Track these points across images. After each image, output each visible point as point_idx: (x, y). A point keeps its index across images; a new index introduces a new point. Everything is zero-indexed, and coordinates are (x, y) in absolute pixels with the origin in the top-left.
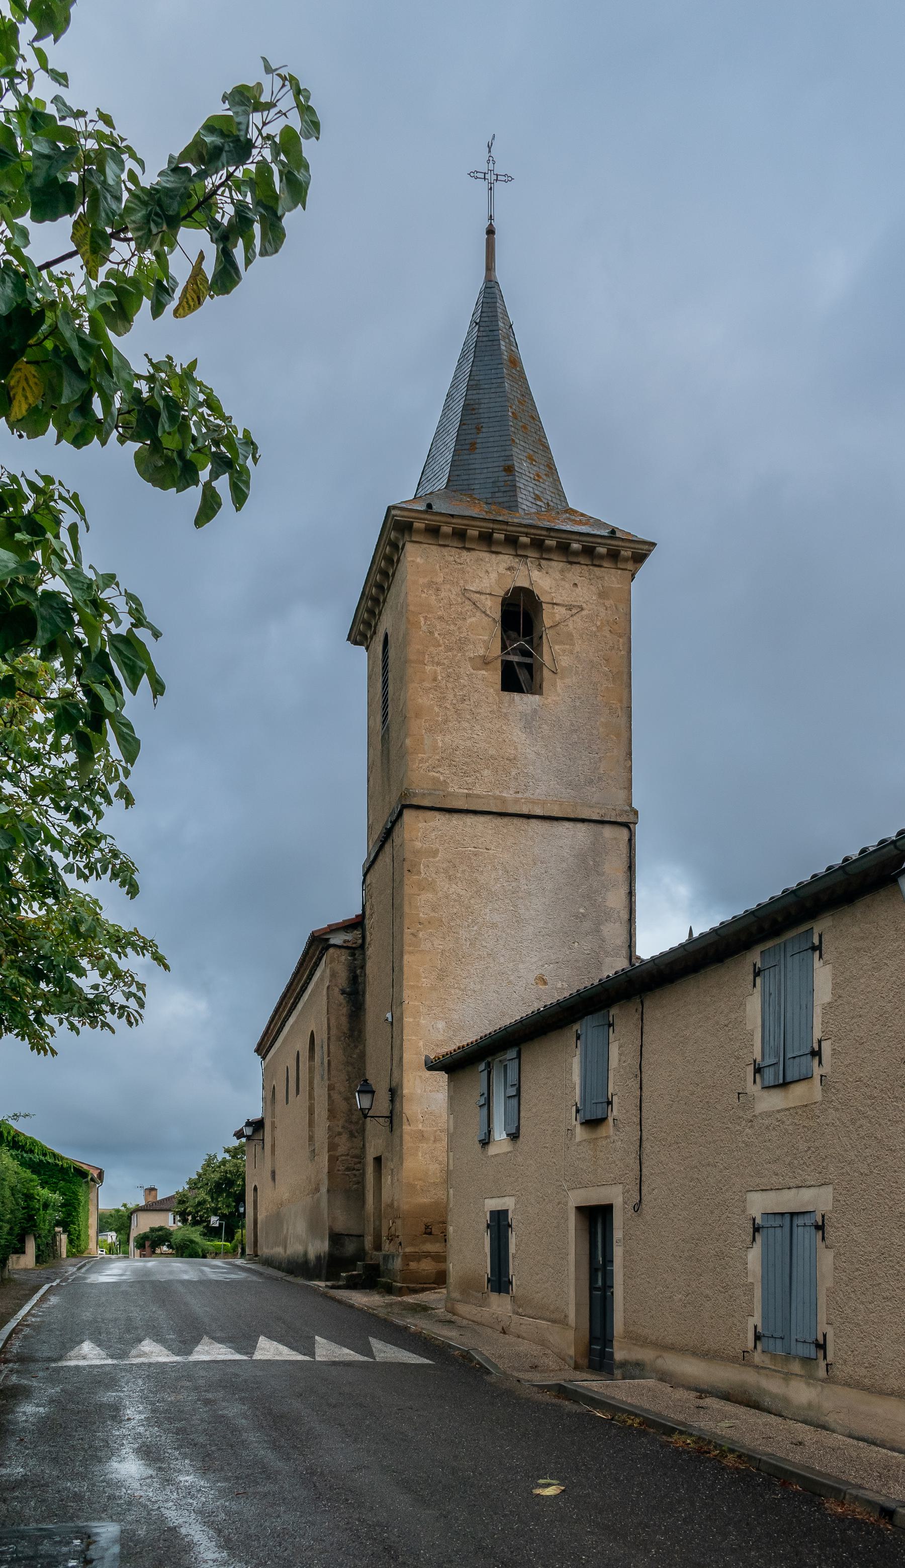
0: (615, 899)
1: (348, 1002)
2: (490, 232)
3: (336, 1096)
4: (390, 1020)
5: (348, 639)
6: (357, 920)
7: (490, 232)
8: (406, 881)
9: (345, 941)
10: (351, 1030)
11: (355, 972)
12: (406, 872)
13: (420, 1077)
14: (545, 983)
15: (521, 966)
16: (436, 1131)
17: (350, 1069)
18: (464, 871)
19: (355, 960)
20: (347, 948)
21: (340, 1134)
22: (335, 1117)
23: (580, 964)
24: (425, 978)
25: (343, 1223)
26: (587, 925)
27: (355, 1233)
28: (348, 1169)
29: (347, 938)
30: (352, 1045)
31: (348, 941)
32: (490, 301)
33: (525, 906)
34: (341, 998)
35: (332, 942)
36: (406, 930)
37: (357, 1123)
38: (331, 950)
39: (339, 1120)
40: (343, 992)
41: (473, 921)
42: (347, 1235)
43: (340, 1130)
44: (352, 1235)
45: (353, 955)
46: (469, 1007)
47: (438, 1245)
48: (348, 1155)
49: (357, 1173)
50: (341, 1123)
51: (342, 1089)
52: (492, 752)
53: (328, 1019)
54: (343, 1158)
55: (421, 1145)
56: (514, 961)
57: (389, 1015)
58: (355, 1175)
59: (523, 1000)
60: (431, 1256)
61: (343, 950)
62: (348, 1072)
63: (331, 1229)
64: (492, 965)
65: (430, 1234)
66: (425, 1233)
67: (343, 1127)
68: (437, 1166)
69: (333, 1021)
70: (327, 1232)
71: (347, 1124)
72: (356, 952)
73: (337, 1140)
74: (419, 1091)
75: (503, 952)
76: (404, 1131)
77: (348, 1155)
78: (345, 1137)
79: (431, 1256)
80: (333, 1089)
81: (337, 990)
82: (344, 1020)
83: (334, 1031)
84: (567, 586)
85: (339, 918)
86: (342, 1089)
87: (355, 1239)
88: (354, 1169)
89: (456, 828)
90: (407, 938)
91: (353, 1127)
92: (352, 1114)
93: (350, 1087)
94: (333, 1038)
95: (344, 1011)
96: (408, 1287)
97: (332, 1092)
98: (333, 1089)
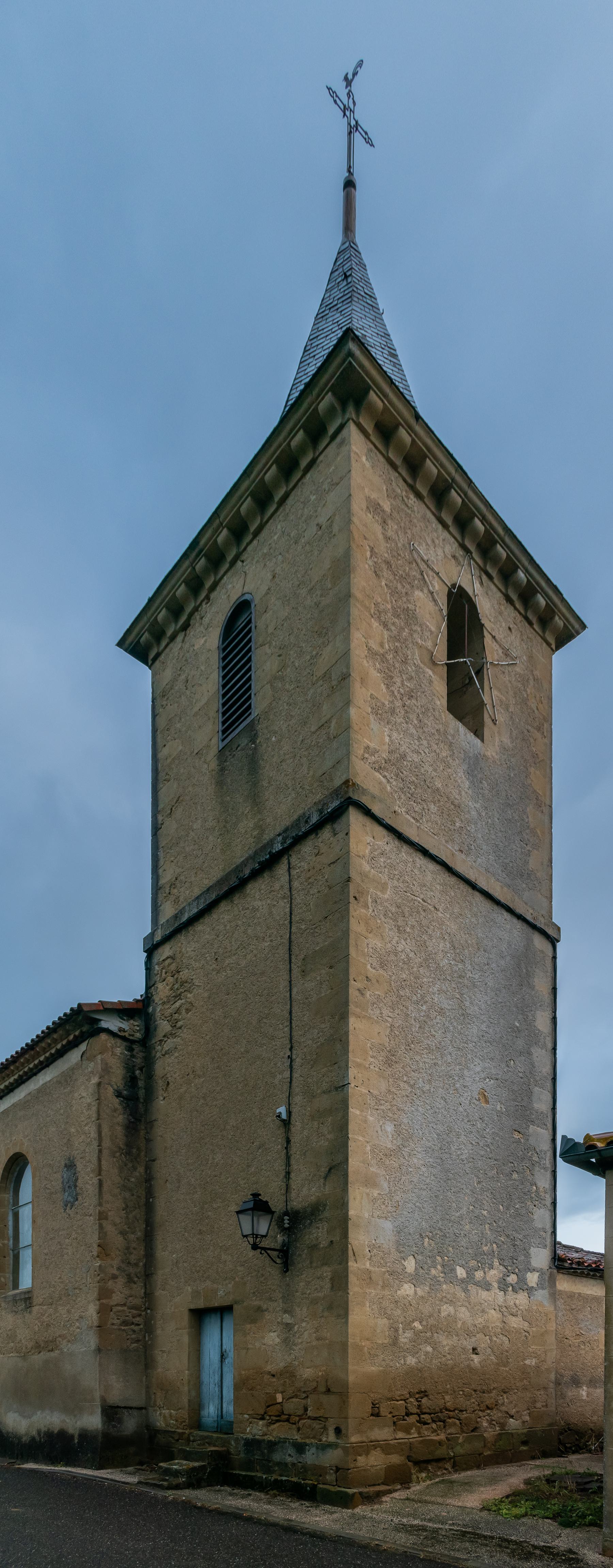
0: (542, 1022)
1: (125, 1108)
2: (349, 184)
3: (109, 1228)
4: (284, 1116)
5: (120, 644)
6: (135, 1006)
7: (349, 184)
8: (352, 912)
9: (121, 1029)
10: (129, 1145)
11: (134, 1073)
12: (352, 900)
13: (368, 1194)
14: (487, 1102)
15: (466, 1072)
16: (384, 1273)
17: (127, 1195)
18: (413, 927)
19: (133, 1056)
20: (124, 1038)
21: (114, 1277)
22: (107, 1255)
23: (515, 1088)
24: (373, 1057)
25: (119, 1390)
26: (520, 1043)
27: (134, 1405)
28: (125, 1323)
29: (123, 1026)
30: (130, 1165)
31: (124, 1031)
32: (347, 277)
33: (470, 998)
34: (116, 1101)
35: (104, 1025)
36: (352, 982)
37: (136, 1265)
38: (103, 1036)
39: (113, 1259)
40: (119, 1094)
41: (423, 997)
42: (125, 1408)
43: (115, 1272)
44: (131, 1408)
45: (131, 1049)
46: (417, 1110)
47: (386, 1430)
48: (124, 1305)
49: (136, 1328)
50: (116, 1262)
51: (118, 1220)
52: (438, 784)
53: (99, 1127)
54: (120, 1308)
55: (368, 1291)
56: (460, 1064)
57: (282, 1110)
58: (134, 1331)
59: (467, 1116)
60: (381, 1446)
61: (119, 1042)
62: (125, 1198)
63: (103, 1399)
64: (440, 1062)
65: (378, 1415)
66: (372, 1415)
67: (119, 1269)
68: (385, 1321)
69: (105, 1131)
70: (98, 1403)
71: (123, 1266)
72: (134, 1046)
73: (110, 1284)
74: (366, 1215)
75: (451, 1049)
76: (350, 1269)
77: (124, 1305)
78: (121, 1281)
79: (381, 1446)
80: (106, 1218)
81: (110, 1090)
82: (119, 1131)
83: (107, 1143)
84: (504, 624)
85: (113, 997)
86: (118, 1220)
87: (135, 1413)
88: (133, 1323)
89: (406, 862)
90: (353, 993)
91: (131, 1270)
92: (131, 1253)
93: (127, 1218)
94: (105, 1152)
95: (121, 1118)
96: (361, 1493)
97: (104, 1223)
98: (106, 1218)
